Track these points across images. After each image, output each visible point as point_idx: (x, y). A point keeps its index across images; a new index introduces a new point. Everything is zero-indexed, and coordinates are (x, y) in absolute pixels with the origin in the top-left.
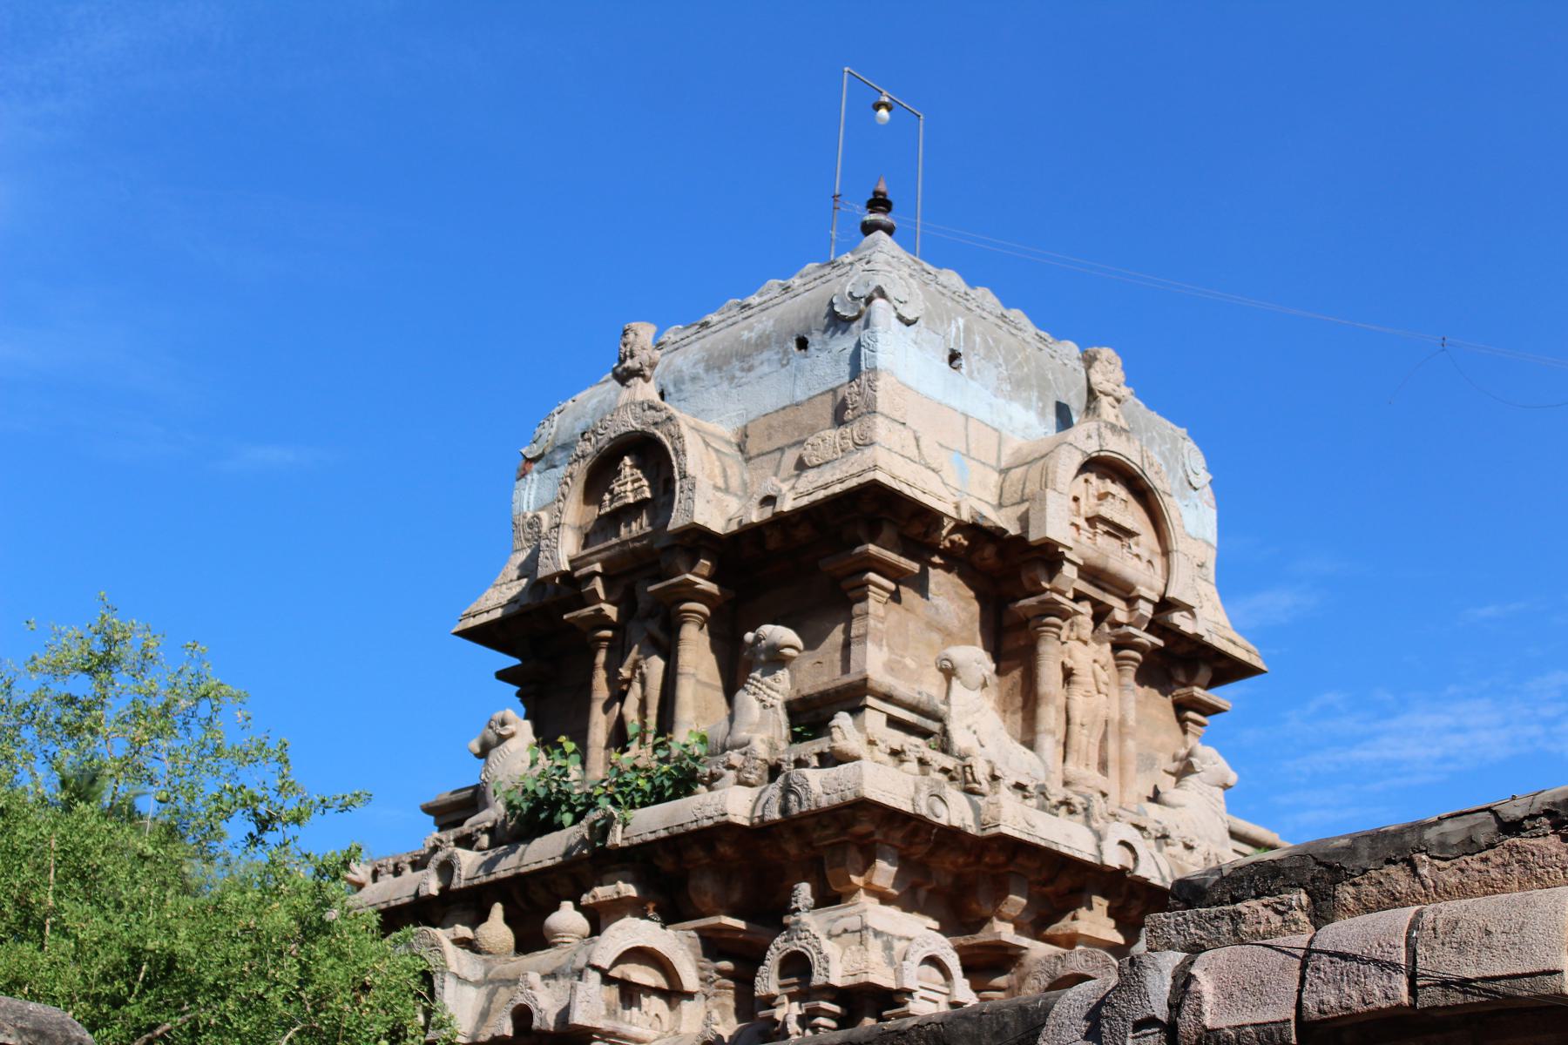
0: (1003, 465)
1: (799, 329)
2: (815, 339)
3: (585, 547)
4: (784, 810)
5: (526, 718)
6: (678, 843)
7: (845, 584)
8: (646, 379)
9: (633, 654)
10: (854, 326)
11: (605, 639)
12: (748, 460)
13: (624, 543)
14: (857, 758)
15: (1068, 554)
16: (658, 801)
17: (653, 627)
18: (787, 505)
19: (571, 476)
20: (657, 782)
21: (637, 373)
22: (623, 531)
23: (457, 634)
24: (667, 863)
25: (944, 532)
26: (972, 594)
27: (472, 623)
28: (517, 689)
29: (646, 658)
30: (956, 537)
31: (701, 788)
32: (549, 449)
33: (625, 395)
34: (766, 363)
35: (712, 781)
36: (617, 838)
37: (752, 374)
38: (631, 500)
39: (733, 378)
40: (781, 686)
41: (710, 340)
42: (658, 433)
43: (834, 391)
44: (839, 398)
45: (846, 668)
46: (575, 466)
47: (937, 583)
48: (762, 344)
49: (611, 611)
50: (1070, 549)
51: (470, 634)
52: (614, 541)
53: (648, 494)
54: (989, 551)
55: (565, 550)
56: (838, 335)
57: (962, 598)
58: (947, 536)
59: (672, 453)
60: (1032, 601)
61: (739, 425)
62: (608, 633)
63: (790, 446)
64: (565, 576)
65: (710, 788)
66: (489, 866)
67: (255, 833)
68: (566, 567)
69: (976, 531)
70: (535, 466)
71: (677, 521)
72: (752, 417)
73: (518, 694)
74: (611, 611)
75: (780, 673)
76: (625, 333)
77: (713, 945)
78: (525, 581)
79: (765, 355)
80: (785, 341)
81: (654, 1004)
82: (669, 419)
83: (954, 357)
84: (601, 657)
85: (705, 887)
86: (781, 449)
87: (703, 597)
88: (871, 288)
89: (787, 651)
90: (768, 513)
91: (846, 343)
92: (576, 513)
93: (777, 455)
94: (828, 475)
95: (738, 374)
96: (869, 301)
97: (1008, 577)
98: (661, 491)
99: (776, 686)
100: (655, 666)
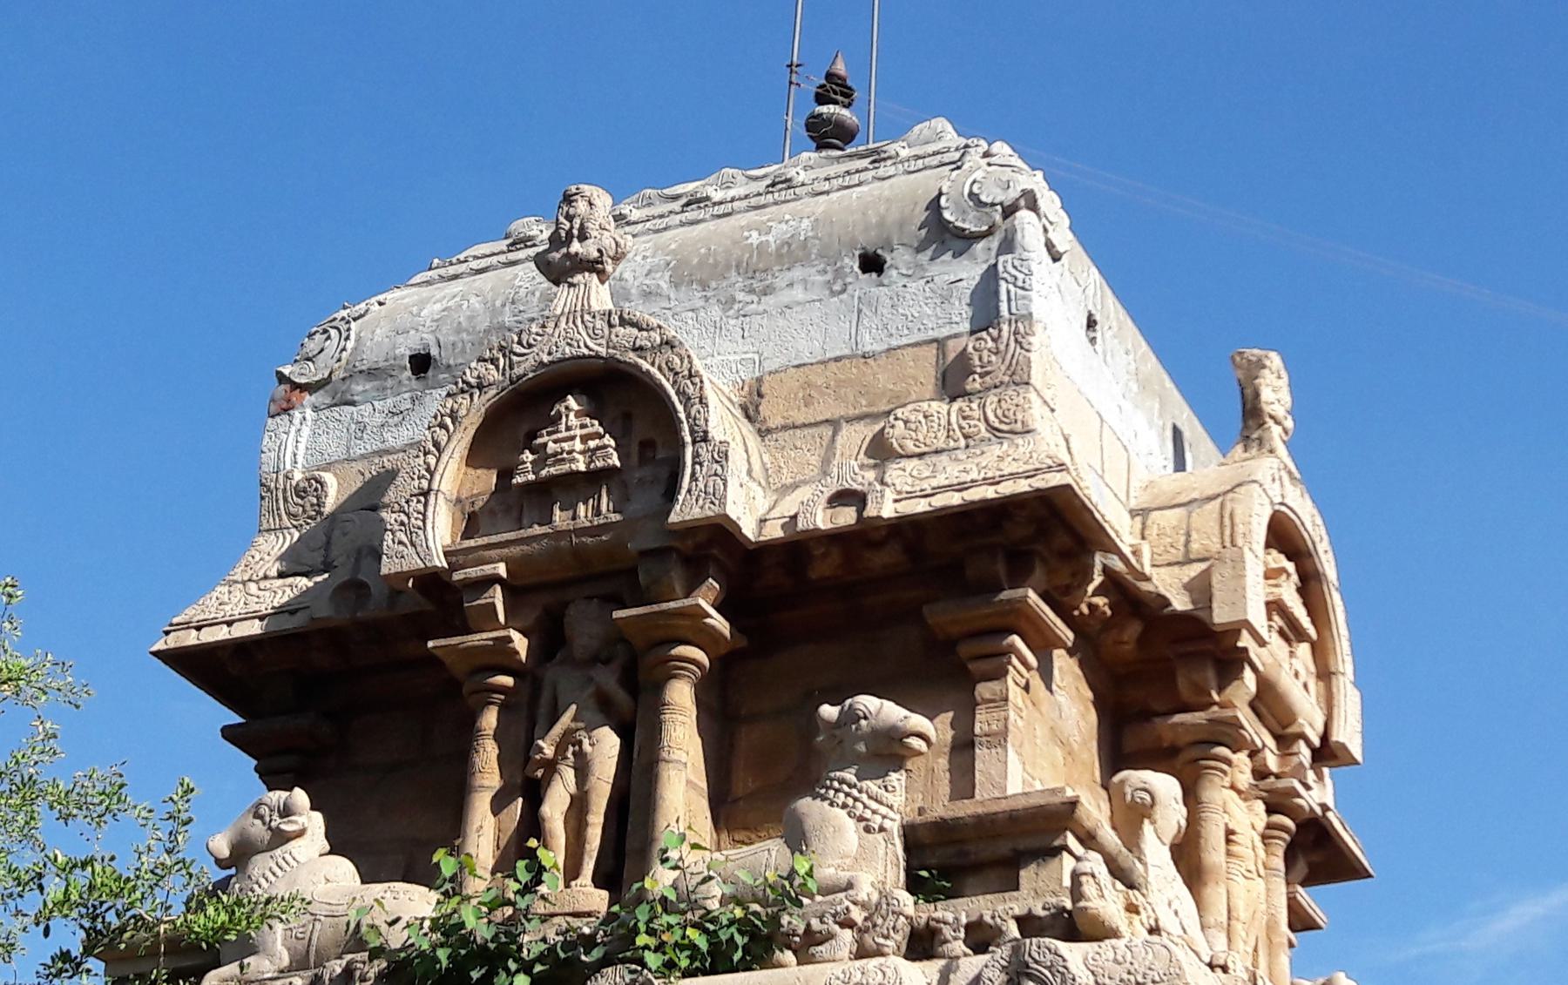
0: (1133, 504)
1: (869, 241)
2: (899, 260)
3: (466, 535)
5: (312, 808)
7: (965, 650)
8: (602, 275)
9: (566, 720)
10: (980, 246)
11: (502, 689)
12: (763, 433)
13: (560, 534)
14: (1114, 934)
15: (1254, 652)
16: (713, 971)
17: (608, 679)
18: (886, 508)
19: (453, 415)
20: (724, 936)
21: (593, 266)
22: (560, 517)
25: (1090, 589)
26: (1090, 695)
27: (191, 638)
28: (255, 762)
29: (590, 729)
30: (1100, 601)
31: (788, 956)
32: (341, 374)
33: (564, 298)
34: (799, 288)
37: (769, 301)
38: (582, 468)
39: (733, 300)
40: (898, 798)
41: (708, 234)
42: (645, 366)
43: (940, 343)
44: (951, 356)
46: (464, 400)
47: (1060, 669)
48: (791, 254)
49: (520, 643)
50: (1262, 643)
51: (180, 660)
52: (537, 530)
53: (615, 461)
54: (1133, 630)
55: (432, 535)
56: (948, 256)
57: (1080, 696)
58: (1092, 598)
59: (675, 398)
60: (1198, 717)
61: (748, 374)
62: (508, 681)
63: (849, 420)
64: (431, 582)
65: (804, 958)
67: (76, 951)
68: (440, 562)
69: (1128, 596)
70: (309, 399)
71: (687, 509)
72: (769, 366)
73: (256, 770)
74: (520, 643)
75: (894, 776)
76: (568, 199)
78: (303, 583)
79: (797, 273)
80: (839, 256)
82: (669, 344)
83: (1091, 324)
84: (490, 719)
86: (834, 424)
87: (705, 638)
88: (1013, 194)
89: (916, 743)
90: (847, 516)
91: (969, 271)
92: (455, 478)
93: (827, 431)
94: (950, 471)
95: (740, 296)
96: (1009, 211)
97: (1161, 676)
98: (635, 459)
99: (889, 798)
100: (606, 746)
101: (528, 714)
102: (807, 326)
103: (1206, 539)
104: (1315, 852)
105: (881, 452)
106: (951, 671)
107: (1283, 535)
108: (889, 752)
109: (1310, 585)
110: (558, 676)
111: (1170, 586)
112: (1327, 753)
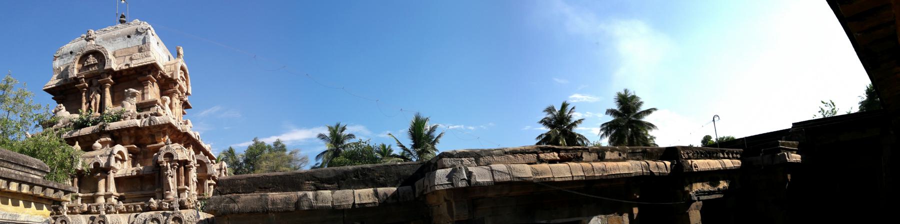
2: (132, 36)
4: (150, 124)
6: (121, 131)
23: (46, 90)
24: (117, 134)
33: (89, 43)
34: (120, 40)
35: (125, 118)
36: (108, 128)
40: (135, 100)
41: (107, 34)
45: (143, 98)
48: (118, 36)
58: (159, 76)
64: (75, 78)
66: (71, 134)
69: (163, 75)
71: (107, 67)
77: (130, 151)
81: (119, 162)
85: (126, 139)
91: (142, 37)
94: (140, 61)
97: (167, 85)
100: (98, 96)
101: (88, 93)
102: (121, 44)
103: (173, 69)
104: (186, 105)
105: (131, 59)
106: (141, 85)
107: (182, 68)
108: (134, 95)
109: (185, 74)
110: (92, 88)
111: (169, 75)
112: (187, 94)
